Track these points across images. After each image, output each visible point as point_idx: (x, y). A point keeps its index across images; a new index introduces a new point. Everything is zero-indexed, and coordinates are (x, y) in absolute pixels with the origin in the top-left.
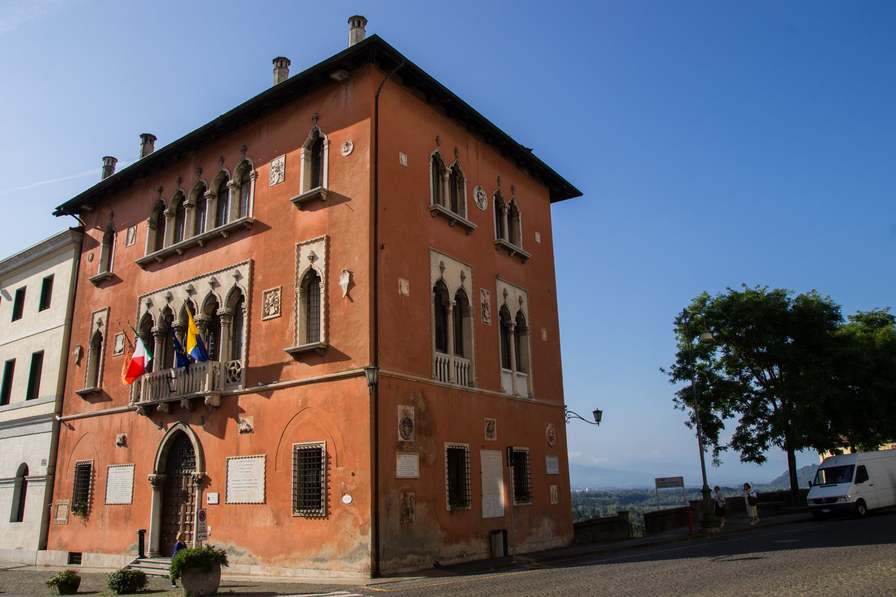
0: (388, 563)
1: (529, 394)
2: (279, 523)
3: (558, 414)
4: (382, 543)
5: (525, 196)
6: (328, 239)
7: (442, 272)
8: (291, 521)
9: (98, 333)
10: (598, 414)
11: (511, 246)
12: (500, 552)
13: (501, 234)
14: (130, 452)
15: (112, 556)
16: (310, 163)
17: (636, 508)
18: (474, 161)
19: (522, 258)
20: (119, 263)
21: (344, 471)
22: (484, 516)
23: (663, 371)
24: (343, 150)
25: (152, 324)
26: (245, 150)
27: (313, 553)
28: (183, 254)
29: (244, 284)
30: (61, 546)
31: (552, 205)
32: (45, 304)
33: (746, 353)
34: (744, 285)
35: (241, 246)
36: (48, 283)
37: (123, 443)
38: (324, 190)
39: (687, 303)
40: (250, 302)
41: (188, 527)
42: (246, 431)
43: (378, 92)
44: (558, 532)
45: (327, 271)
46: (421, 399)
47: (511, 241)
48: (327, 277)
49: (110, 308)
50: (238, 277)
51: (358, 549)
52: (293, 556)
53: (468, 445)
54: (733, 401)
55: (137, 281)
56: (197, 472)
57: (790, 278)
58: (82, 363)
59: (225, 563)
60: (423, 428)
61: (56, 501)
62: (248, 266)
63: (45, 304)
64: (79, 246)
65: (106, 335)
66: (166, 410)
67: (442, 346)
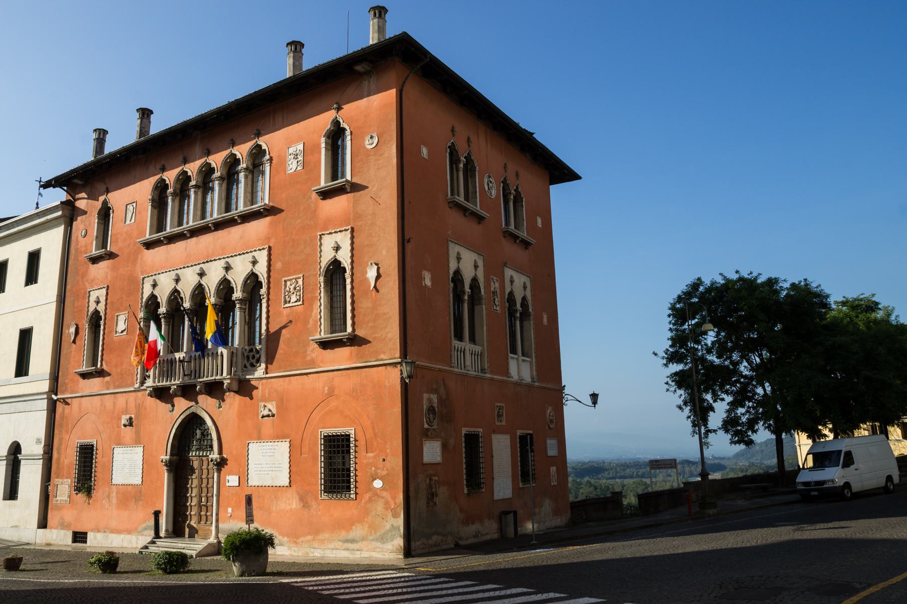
0: (418, 543)
1: (532, 378)
2: (305, 504)
4: (412, 525)
5: (527, 180)
6: (353, 230)
8: (319, 504)
9: (96, 312)
10: (594, 397)
11: (517, 232)
13: (507, 223)
14: (137, 433)
15: (122, 536)
16: (330, 152)
17: (593, 481)
18: (487, 153)
19: (526, 244)
20: (117, 241)
21: (375, 457)
22: (496, 498)
23: (656, 354)
25: (158, 305)
27: (343, 534)
30: (63, 526)
31: (553, 188)
32: (32, 277)
33: (735, 338)
34: (737, 272)
36: (34, 258)
37: (130, 423)
38: (347, 181)
39: (680, 287)
40: (269, 288)
41: (204, 508)
43: (403, 86)
44: (557, 512)
46: (442, 387)
47: (467, 198)
51: (390, 530)
52: (321, 537)
53: (481, 430)
54: (722, 387)
55: (139, 260)
56: (215, 455)
57: (782, 264)
59: (272, 544)
60: (443, 414)
61: (55, 480)
62: (265, 252)
63: (32, 277)
67: (459, 337)
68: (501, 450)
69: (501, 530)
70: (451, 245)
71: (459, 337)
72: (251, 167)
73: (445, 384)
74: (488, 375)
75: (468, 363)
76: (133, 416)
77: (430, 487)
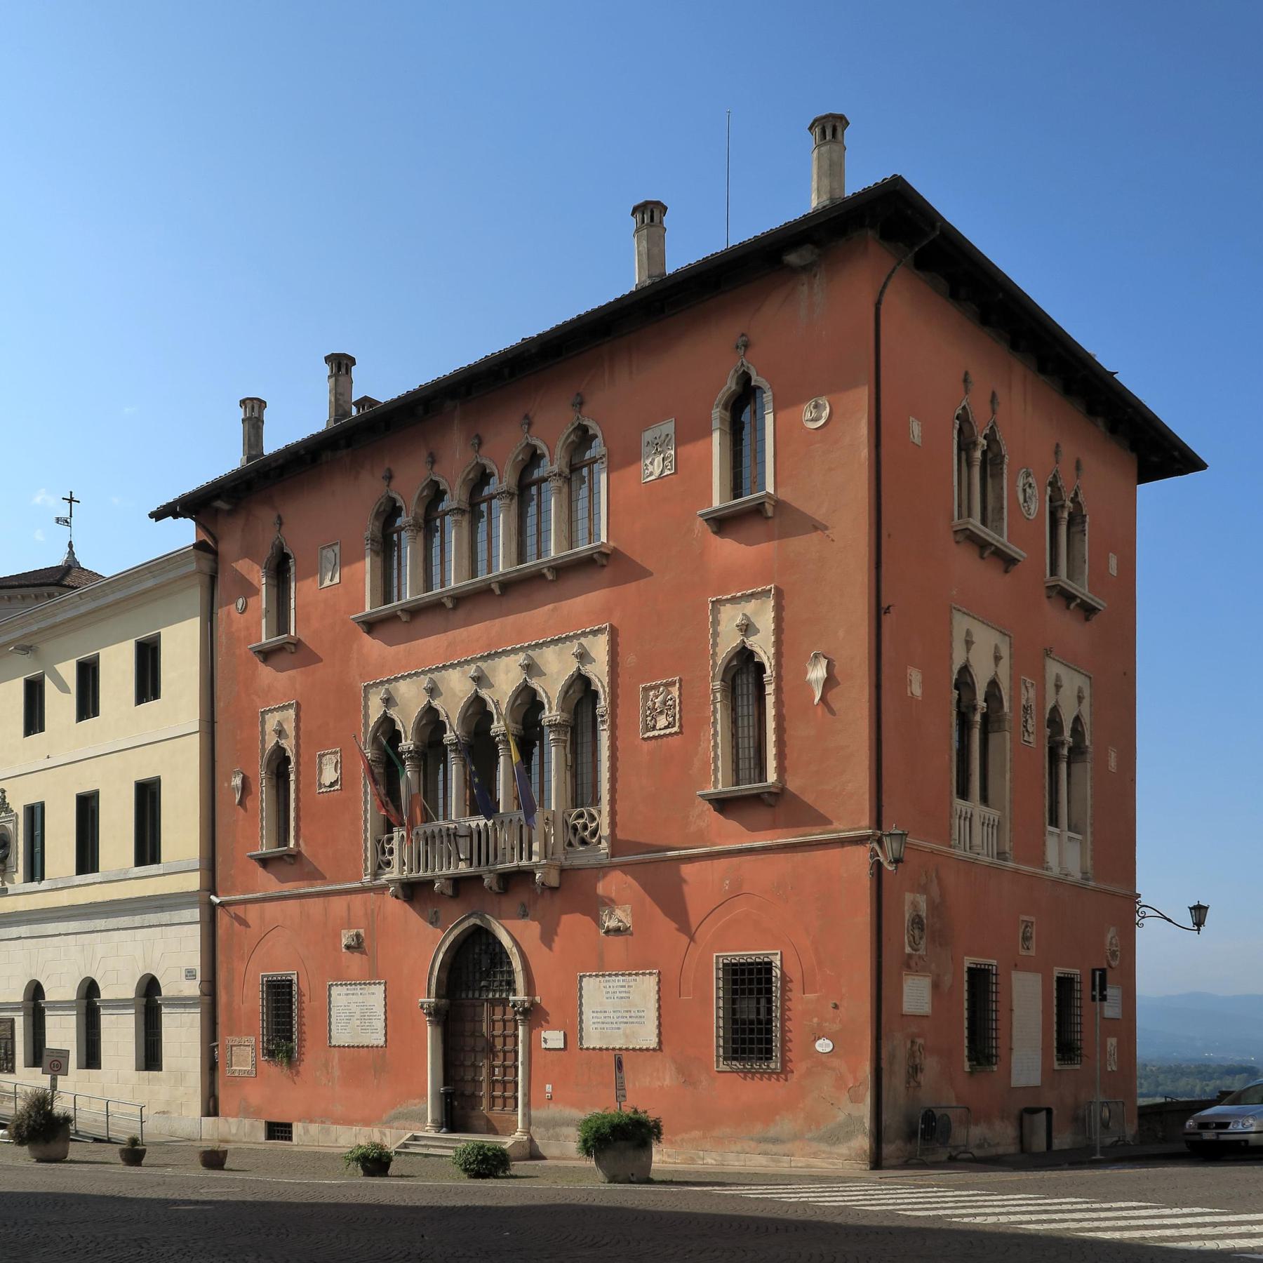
1: (1084, 873)
3: (1123, 909)
6: (779, 595)
7: (968, 650)
9: (279, 751)
10: (1199, 913)
12: (1039, 1143)
13: (1054, 570)
16: (728, 437)
18: (1032, 427)
19: (1088, 611)
24: (808, 416)
26: (580, 404)
28: (455, 608)
29: (598, 672)
30: (246, 1111)
31: (1142, 489)
35: (586, 602)
37: (357, 946)
38: (768, 495)
42: (617, 931)
43: (882, 293)
45: (778, 655)
46: (935, 881)
47: (984, 521)
48: (778, 665)
49: (298, 703)
50: (583, 656)
58: (249, 804)
61: (224, 1039)
62: (603, 639)
63: (148, 684)
64: (207, 579)
65: (298, 755)
66: (449, 892)
68: (1026, 1004)
69: (1021, 1142)
70: (957, 617)
71: (963, 793)
72: (567, 471)
73: (938, 877)
74: (1010, 864)
75: (977, 840)
76: (362, 931)
77: (912, 1055)
